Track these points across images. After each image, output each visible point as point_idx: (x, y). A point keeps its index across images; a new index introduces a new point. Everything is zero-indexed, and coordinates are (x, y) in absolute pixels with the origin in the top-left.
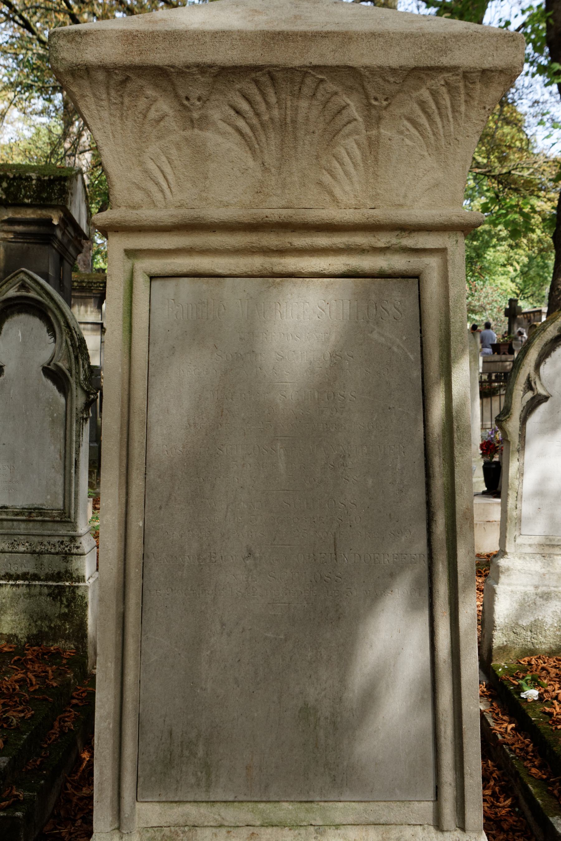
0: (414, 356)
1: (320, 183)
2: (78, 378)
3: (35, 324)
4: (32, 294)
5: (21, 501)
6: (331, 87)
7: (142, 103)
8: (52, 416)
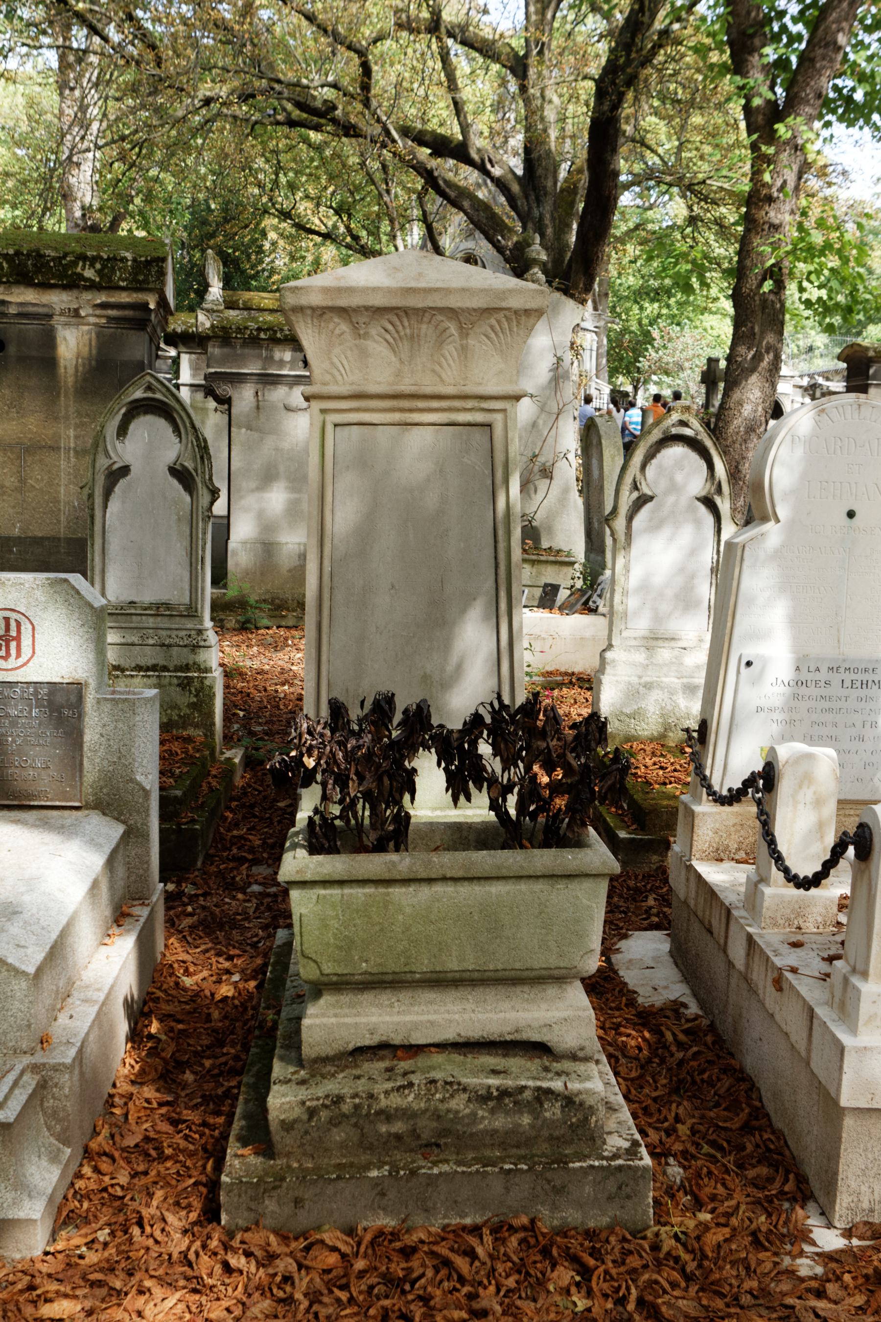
0: (488, 472)
1: (433, 371)
2: (203, 478)
3: (161, 424)
4: (158, 396)
5: (148, 597)
6: (440, 318)
7: (331, 326)
8: (178, 514)
